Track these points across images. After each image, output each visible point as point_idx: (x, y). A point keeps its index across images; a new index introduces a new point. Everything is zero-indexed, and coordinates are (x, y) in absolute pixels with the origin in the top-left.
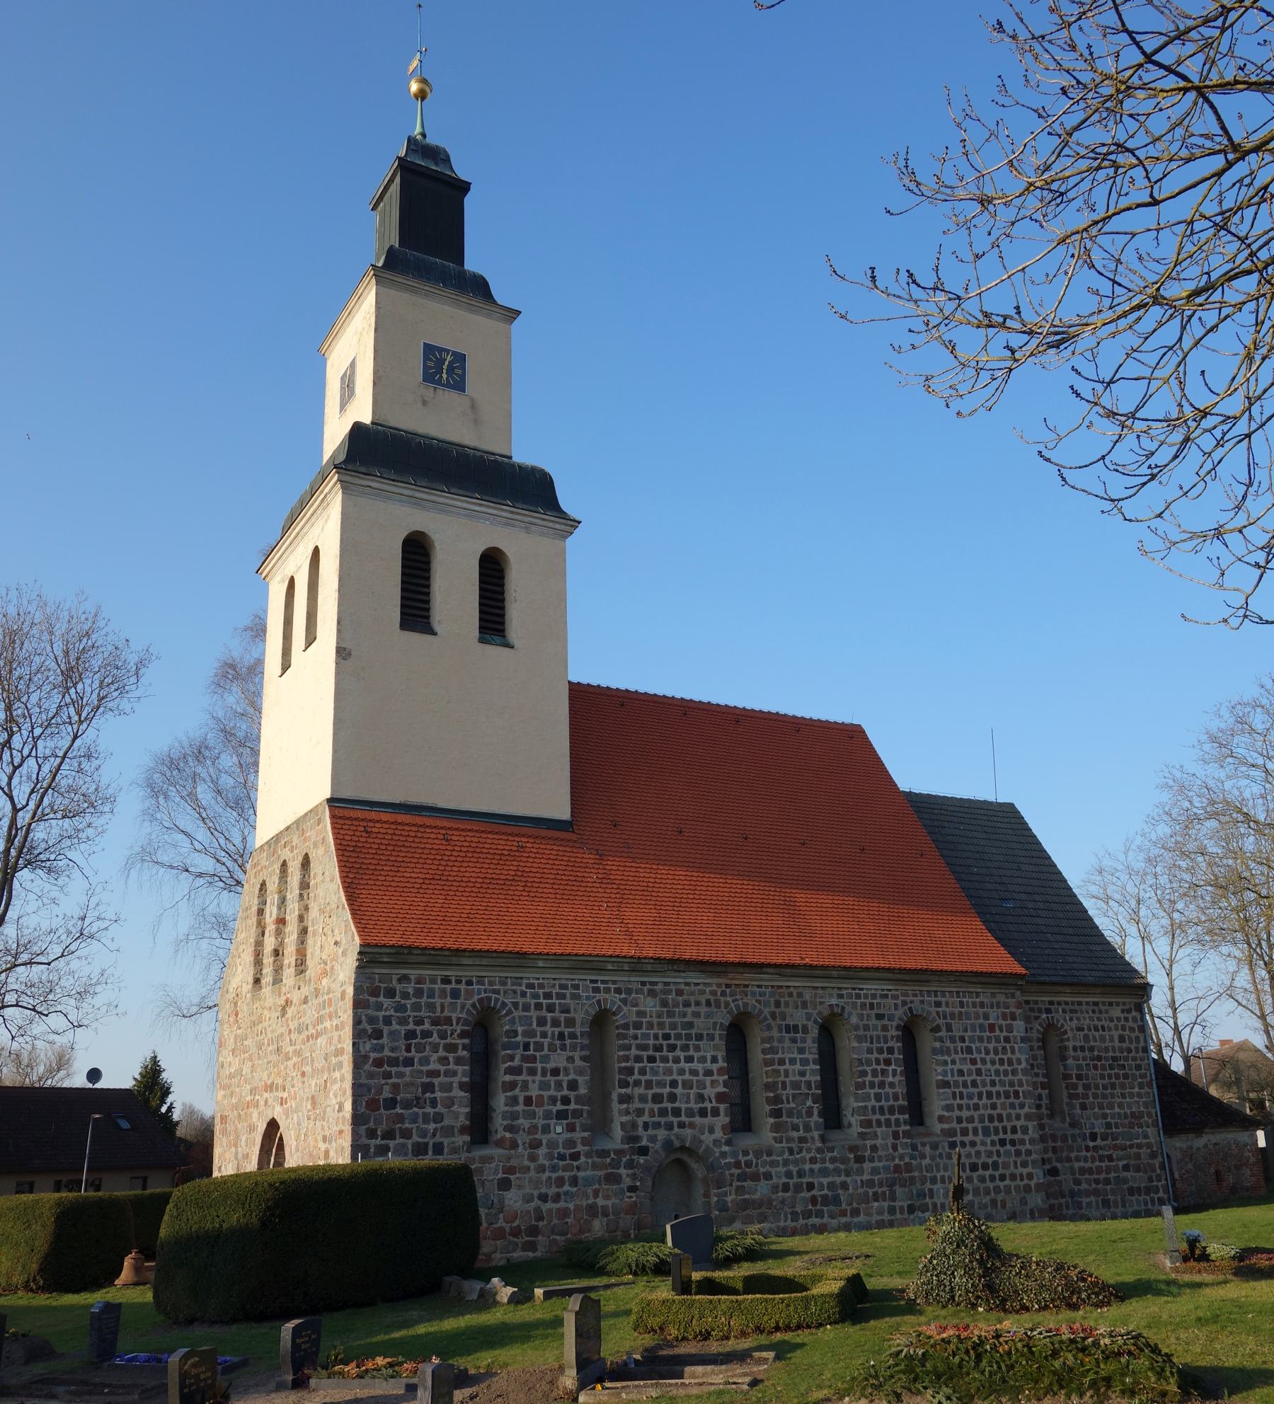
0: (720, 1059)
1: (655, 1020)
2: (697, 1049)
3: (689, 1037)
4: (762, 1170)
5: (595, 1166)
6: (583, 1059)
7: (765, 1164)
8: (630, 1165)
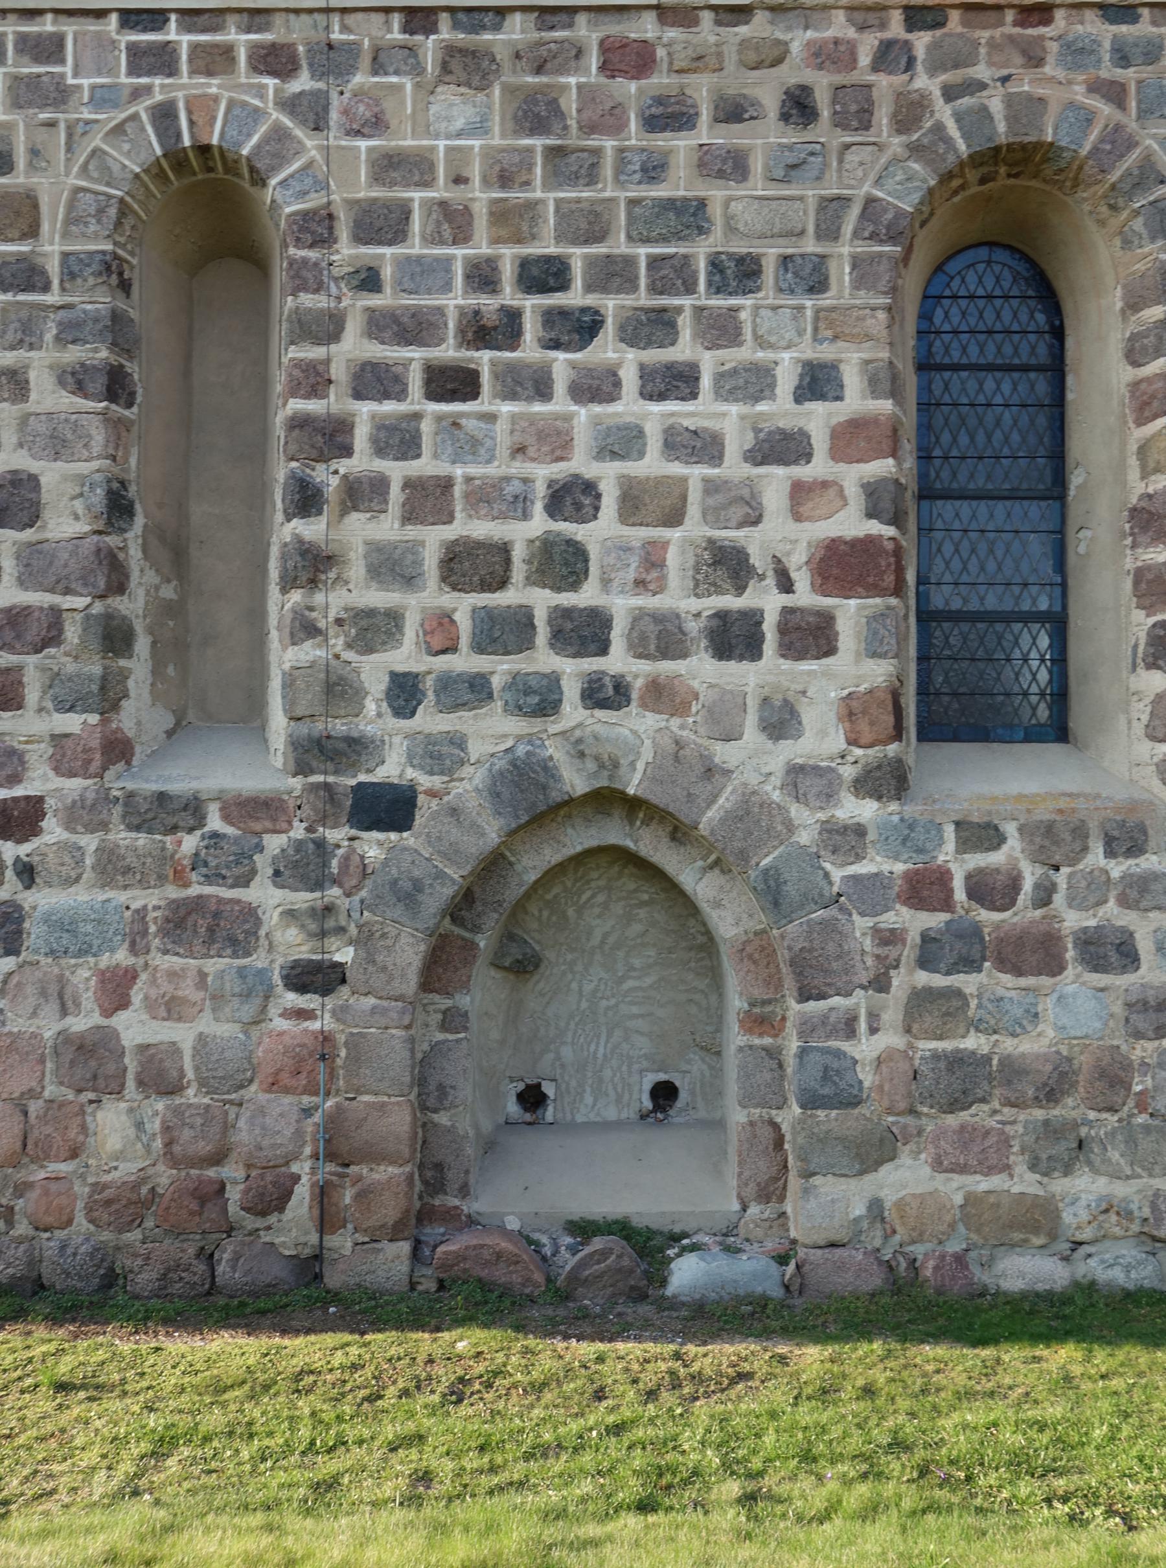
0: (852, 379)
1: (480, 197)
2: (721, 330)
3: (673, 275)
4: (1073, 920)
5: (113, 869)
6: (75, 380)
7: (1093, 890)
8: (308, 867)
